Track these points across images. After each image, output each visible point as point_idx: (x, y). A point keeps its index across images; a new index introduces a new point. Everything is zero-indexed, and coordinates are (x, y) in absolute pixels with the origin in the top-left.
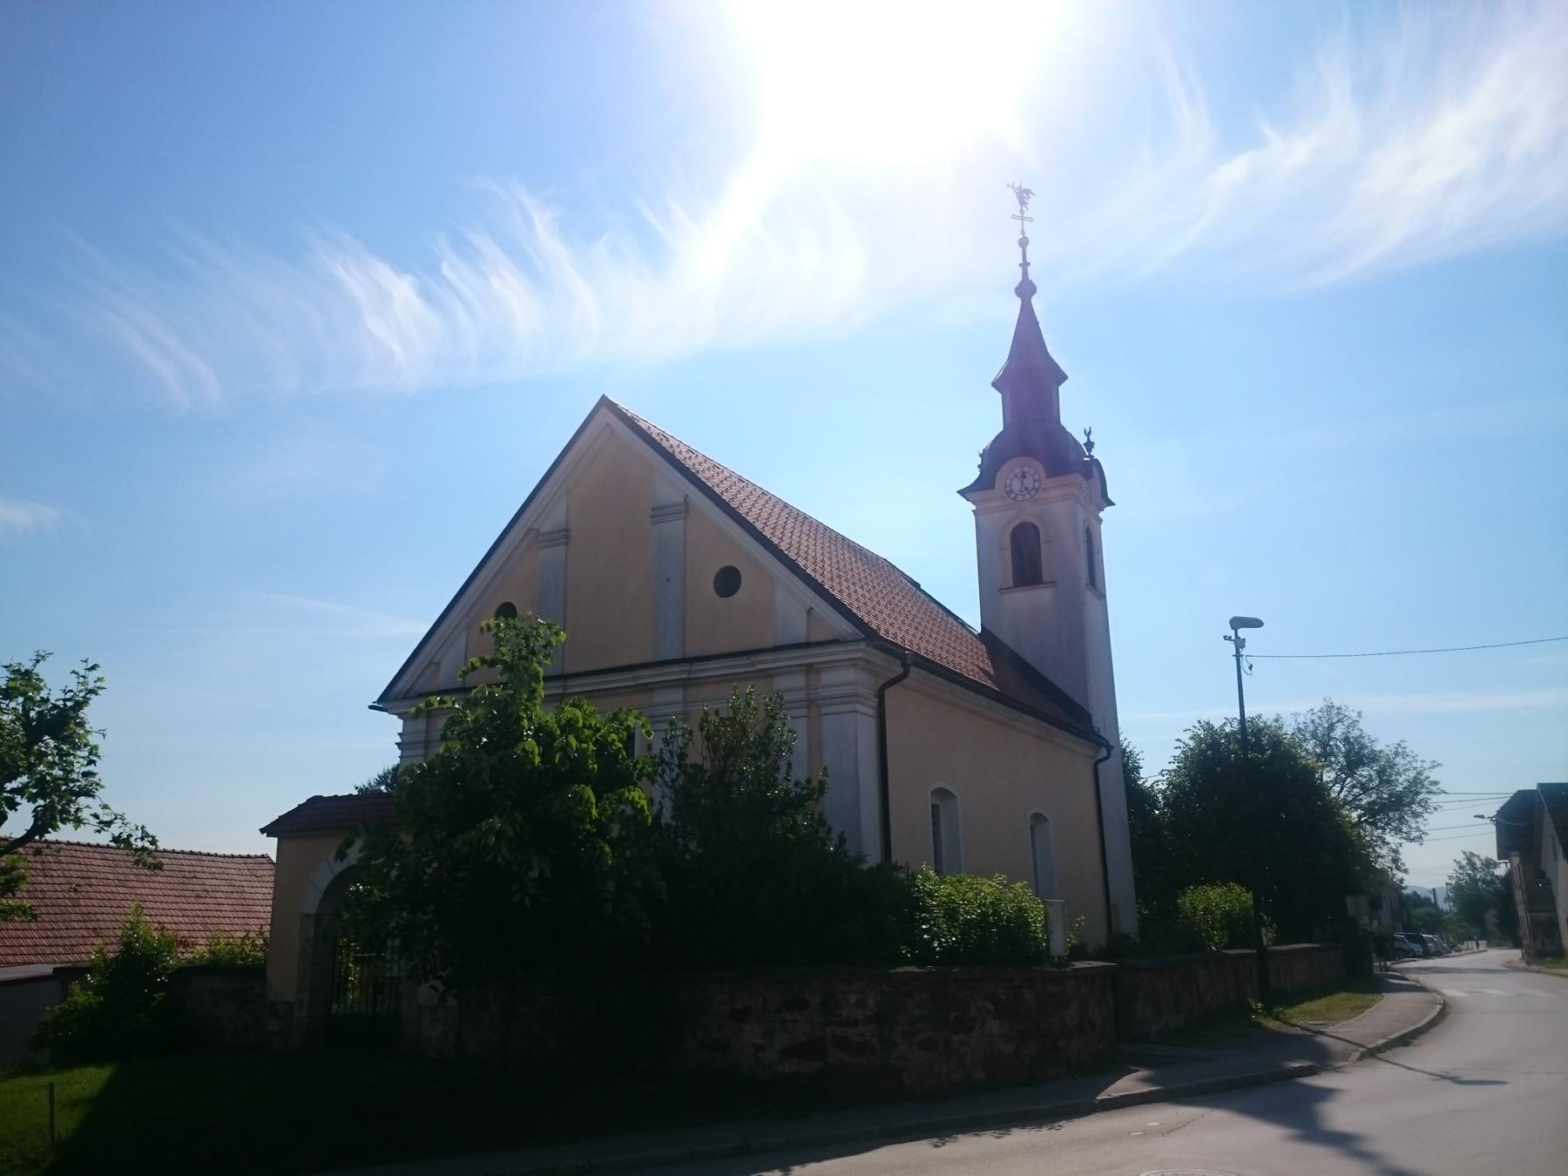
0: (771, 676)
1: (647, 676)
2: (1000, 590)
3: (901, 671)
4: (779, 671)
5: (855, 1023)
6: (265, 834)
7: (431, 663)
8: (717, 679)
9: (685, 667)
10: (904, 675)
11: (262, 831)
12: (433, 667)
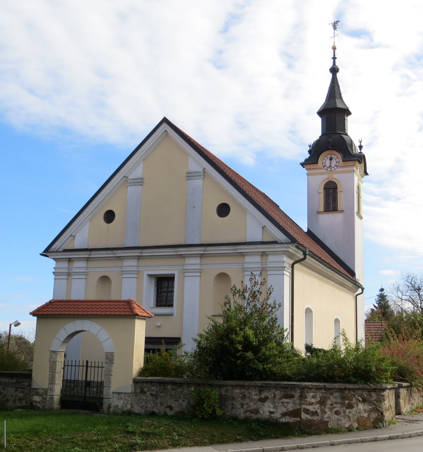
0: (244, 256)
1: (120, 253)
2: (318, 212)
3: (302, 257)
4: (248, 253)
5: (312, 404)
6: (32, 315)
7: (71, 236)
8: (234, 254)
9: (203, 248)
10: (305, 258)
11: (31, 314)
12: (72, 237)
